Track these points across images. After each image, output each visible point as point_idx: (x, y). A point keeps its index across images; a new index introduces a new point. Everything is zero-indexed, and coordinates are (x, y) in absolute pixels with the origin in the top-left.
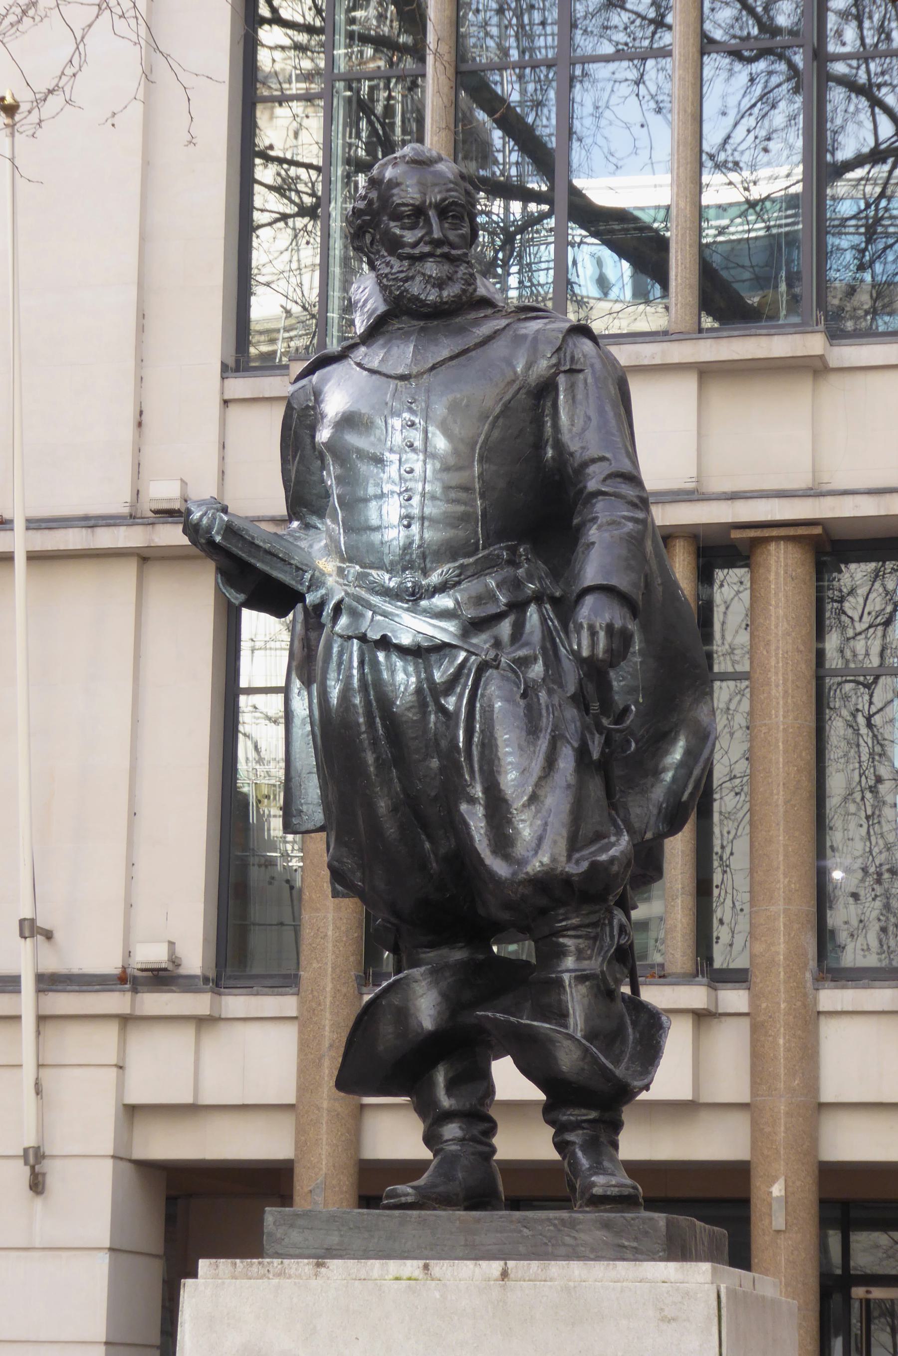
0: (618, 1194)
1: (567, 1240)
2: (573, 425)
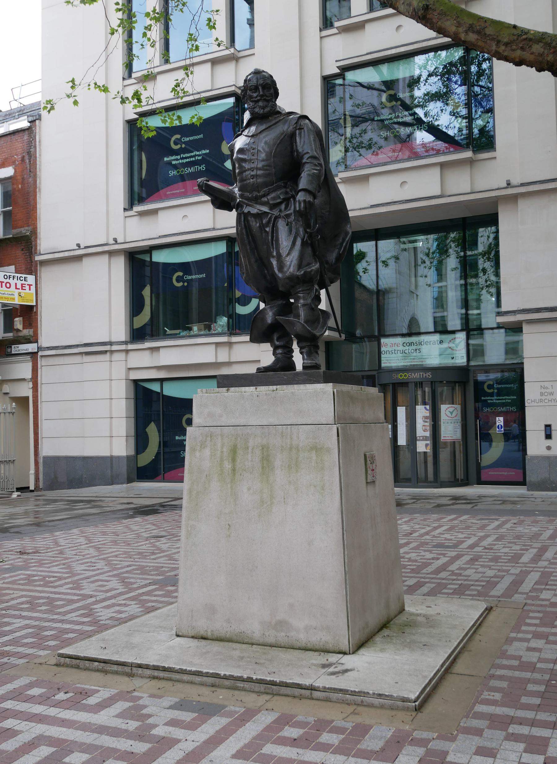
1: (296, 379)
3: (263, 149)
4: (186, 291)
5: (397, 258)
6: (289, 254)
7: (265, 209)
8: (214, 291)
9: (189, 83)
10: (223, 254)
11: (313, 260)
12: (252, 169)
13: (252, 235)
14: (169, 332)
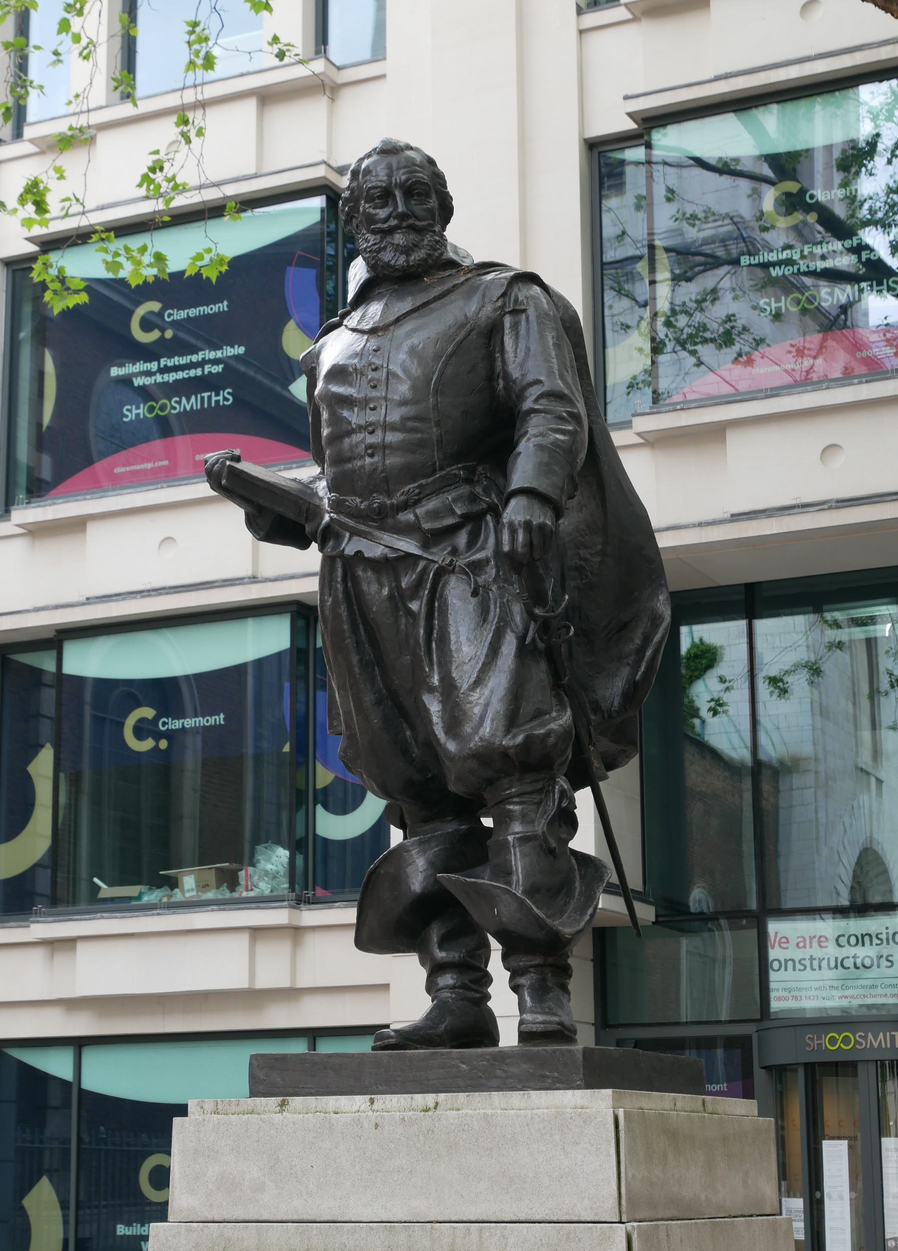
0: (543, 1030)
2: (516, 357)
3: (405, 370)
4: (164, 766)
5: (815, 670)
6: (478, 682)
7: (408, 546)
8: (249, 764)
9: (192, 161)
10: (279, 654)
11: (554, 702)
12: (369, 428)
13: (366, 623)
14: (106, 890)
